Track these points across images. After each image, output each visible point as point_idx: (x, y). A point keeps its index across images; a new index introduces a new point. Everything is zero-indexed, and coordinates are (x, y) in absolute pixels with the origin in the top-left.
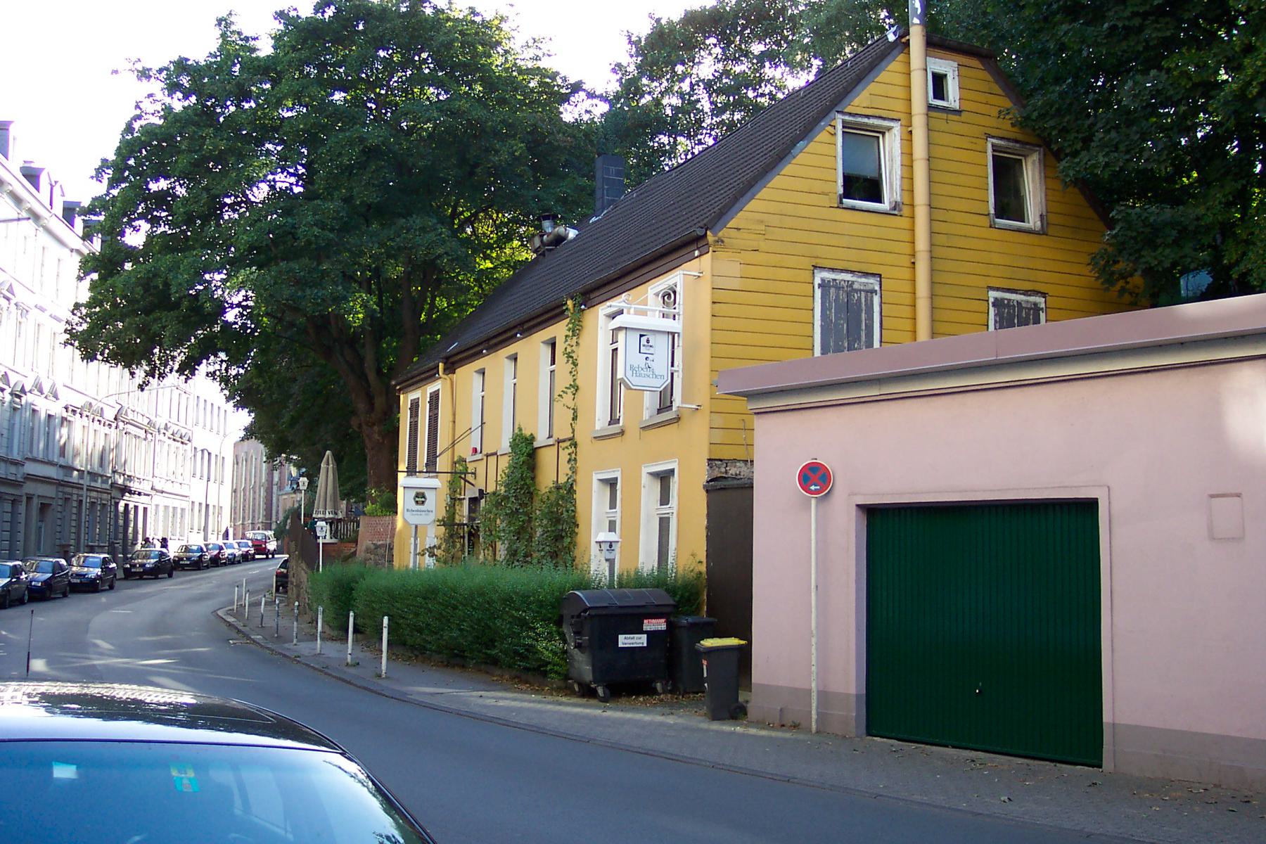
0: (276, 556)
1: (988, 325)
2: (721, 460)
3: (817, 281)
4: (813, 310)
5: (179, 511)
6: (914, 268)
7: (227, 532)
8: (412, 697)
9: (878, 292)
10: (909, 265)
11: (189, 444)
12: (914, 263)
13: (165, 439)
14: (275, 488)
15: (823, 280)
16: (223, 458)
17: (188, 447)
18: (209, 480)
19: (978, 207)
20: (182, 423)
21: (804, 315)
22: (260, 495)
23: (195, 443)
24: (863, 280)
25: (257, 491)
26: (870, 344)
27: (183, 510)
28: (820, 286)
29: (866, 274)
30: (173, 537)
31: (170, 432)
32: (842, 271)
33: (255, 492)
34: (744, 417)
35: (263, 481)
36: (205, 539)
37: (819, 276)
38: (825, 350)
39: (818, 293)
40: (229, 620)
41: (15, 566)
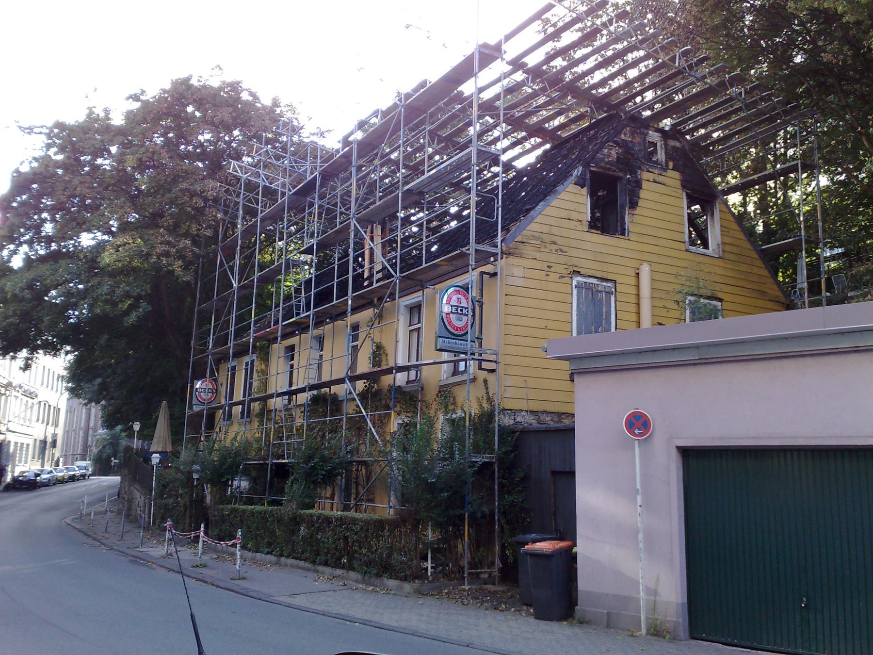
0: (90, 477)
1: (685, 320)
2: (511, 410)
3: (575, 283)
4: (571, 303)
5: (25, 446)
6: (638, 277)
7: (58, 459)
8: (274, 598)
9: (614, 293)
10: (634, 275)
11: (36, 399)
12: (638, 274)
13: (19, 395)
14: (91, 432)
15: (578, 283)
16: (59, 409)
17: (35, 401)
18: (47, 424)
19: (677, 236)
20: (32, 384)
21: (565, 307)
22: (79, 435)
23: (40, 398)
24: (604, 284)
25: (78, 433)
26: (608, 330)
27: (28, 445)
28: (576, 287)
29: (607, 280)
30: (19, 464)
31: (23, 390)
32: (590, 276)
33: (75, 434)
34: (526, 379)
35: (82, 425)
36: (43, 466)
37: (577, 279)
38: (579, 333)
39: (575, 291)
40: (77, 527)
41: (125, 515)
